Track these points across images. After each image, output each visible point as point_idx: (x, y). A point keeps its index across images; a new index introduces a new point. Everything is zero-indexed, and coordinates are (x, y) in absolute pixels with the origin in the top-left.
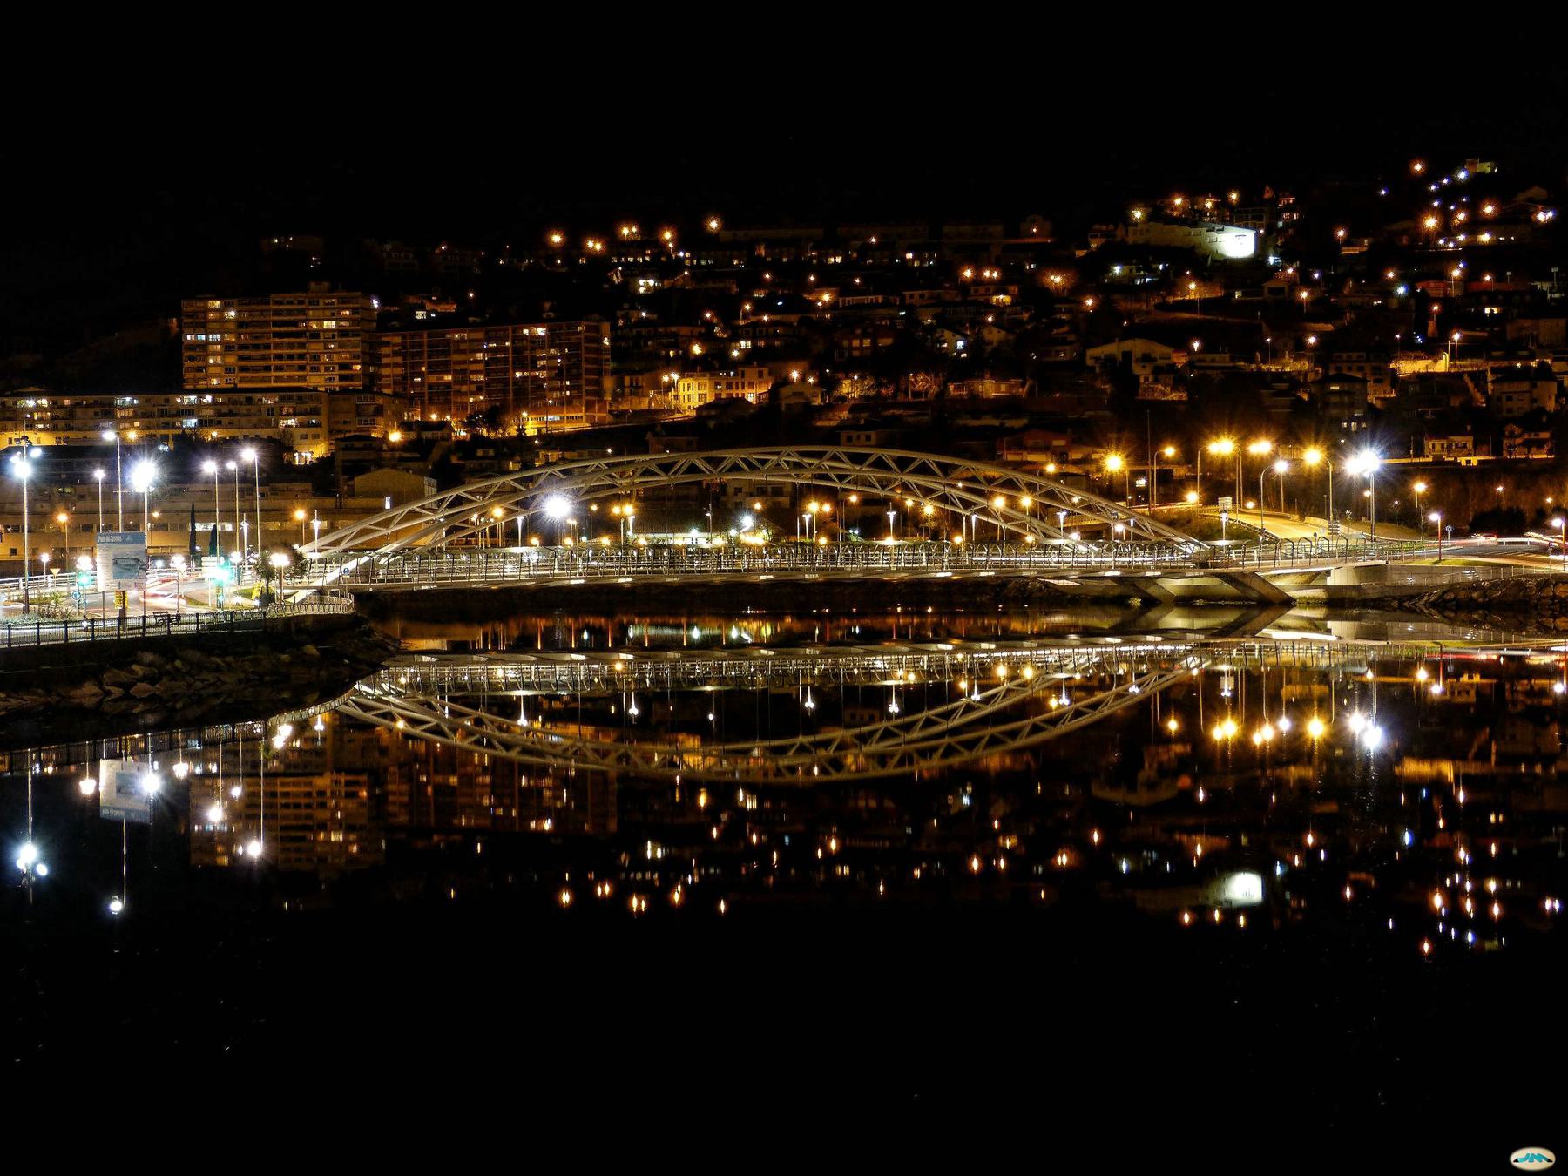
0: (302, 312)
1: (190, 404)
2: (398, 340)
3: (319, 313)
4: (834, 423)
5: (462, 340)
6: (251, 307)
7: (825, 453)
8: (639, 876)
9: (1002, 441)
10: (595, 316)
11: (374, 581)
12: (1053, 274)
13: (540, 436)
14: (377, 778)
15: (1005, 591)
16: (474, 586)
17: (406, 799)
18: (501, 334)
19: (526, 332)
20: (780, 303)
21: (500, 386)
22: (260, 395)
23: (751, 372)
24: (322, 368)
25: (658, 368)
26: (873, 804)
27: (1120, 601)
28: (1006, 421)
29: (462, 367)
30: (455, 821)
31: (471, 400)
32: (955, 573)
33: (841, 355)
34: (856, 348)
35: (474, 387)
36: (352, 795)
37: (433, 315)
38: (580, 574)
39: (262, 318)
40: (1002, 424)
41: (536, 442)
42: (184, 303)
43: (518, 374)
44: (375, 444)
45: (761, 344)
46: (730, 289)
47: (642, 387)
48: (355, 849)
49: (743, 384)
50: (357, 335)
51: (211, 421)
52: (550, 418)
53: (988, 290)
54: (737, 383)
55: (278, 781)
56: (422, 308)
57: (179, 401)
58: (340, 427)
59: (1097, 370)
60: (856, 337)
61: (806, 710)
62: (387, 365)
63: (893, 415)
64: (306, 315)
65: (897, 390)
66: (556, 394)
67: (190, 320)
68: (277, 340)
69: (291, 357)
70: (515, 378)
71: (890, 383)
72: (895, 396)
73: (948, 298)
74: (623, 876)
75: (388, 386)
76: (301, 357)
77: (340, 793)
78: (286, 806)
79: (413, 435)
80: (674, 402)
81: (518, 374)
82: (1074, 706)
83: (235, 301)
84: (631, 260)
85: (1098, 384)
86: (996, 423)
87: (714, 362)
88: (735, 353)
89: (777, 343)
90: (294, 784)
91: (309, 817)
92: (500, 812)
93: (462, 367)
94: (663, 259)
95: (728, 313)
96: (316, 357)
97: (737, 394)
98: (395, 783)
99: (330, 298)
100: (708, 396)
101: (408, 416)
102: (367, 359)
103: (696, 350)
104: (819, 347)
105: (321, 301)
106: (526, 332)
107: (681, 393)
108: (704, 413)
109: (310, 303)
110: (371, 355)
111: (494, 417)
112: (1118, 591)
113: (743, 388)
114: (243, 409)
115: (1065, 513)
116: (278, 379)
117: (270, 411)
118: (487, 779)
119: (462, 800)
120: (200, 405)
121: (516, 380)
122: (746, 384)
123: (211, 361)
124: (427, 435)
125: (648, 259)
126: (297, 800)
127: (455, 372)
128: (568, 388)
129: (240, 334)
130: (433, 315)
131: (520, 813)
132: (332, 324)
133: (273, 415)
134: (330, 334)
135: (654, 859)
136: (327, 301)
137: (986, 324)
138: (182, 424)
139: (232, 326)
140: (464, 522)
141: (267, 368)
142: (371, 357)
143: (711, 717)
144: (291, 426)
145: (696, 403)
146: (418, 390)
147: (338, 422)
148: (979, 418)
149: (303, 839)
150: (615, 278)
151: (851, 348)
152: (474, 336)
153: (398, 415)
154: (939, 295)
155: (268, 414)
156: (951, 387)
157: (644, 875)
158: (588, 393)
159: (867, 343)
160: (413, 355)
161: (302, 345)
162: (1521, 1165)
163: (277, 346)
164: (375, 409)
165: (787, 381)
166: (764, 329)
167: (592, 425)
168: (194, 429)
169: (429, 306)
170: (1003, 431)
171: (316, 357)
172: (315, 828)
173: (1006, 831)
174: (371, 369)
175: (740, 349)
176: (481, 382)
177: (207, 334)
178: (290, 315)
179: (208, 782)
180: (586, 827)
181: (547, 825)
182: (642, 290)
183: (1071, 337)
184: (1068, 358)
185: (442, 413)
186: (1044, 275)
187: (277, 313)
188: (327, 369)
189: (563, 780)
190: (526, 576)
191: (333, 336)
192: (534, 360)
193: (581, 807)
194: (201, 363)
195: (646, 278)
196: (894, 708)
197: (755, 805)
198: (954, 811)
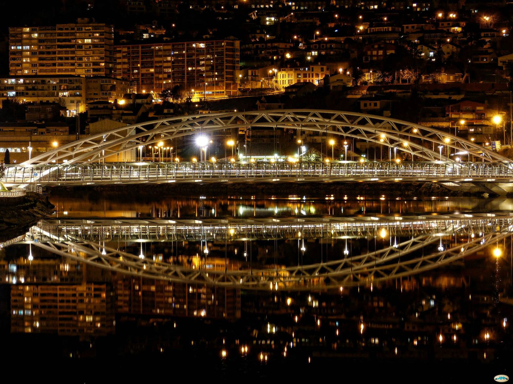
0: (73, 34)
1: (12, 84)
2: (125, 49)
3: (83, 35)
4: (359, 96)
5: (160, 50)
6: (45, 32)
7: (309, 113)
8: (263, 342)
9: (449, 107)
10: (232, 37)
11: (61, 180)
12: (485, 16)
13: (201, 103)
14: (111, 286)
15: (421, 189)
16: (115, 183)
17: (127, 298)
18: (181, 47)
19: (194, 45)
20: (336, 31)
21: (180, 75)
22: (49, 79)
23: (317, 69)
24: (84, 65)
25: (266, 66)
26: (381, 304)
27: (479, 195)
28: (452, 96)
29: (161, 64)
30: (154, 311)
31: (164, 82)
32: (381, 179)
33: (367, 59)
34: (375, 56)
35: (166, 76)
36: (97, 296)
37: (152, 36)
38: (174, 177)
39: (52, 38)
40: (450, 98)
41: (197, 106)
42: (10, 29)
43: (190, 69)
44: (109, 106)
45: (323, 53)
46: (316, 23)
47: (258, 76)
48: (99, 325)
49: (313, 74)
50: (103, 47)
51: (23, 93)
52: (207, 92)
53: (449, 24)
54: (309, 74)
55: (58, 287)
56: (146, 32)
57: (6, 82)
58: (93, 96)
59: (504, 69)
60: (375, 49)
61: (301, 252)
62: (120, 63)
63: (391, 92)
64: (75, 36)
65: (394, 78)
66: (210, 80)
67: (14, 38)
68: (59, 49)
69: (67, 58)
70: (188, 70)
71: (390, 75)
72: (392, 81)
73: (427, 28)
74: (255, 342)
75: (120, 75)
76: (72, 58)
77: (91, 295)
78: (62, 301)
79: (131, 101)
80: (275, 84)
81: (190, 69)
82: (446, 251)
83: (38, 28)
84: (262, 6)
85: (504, 76)
86: (447, 97)
87: (297, 63)
88: (309, 58)
89: (332, 53)
90: (67, 289)
91: (75, 307)
92: (178, 306)
93: (161, 64)
94: (280, 6)
95: (307, 35)
96: (80, 59)
97: (309, 80)
98: (121, 289)
99: (89, 26)
100: (293, 81)
101: (130, 91)
102: (108, 60)
103: (288, 56)
104: (355, 55)
105: (83, 28)
106: (194, 45)
107: (279, 79)
108: (290, 90)
109: (78, 29)
110: (110, 58)
111: (176, 92)
112: (477, 189)
113: (313, 77)
114: (40, 87)
115: (442, 147)
116: (59, 70)
117: (55, 88)
118: (171, 288)
119: (157, 300)
120: (17, 84)
121: (188, 72)
122: (314, 75)
123: (24, 61)
124: (139, 101)
125: (271, 6)
126: (68, 298)
127: (156, 67)
128: (217, 76)
129: (40, 46)
130: (152, 36)
131: (188, 307)
132: (89, 41)
133: (56, 90)
134: (88, 47)
135: (271, 333)
136: (87, 28)
137: (445, 43)
138: (7, 94)
139: (36, 41)
140: (432, 239)
141: (54, 65)
142: (110, 59)
143: (245, 254)
144: (65, 96)
145: (287, 85)
146: (136, 77)
147: (91, 94)
148: (437, 94)
149: (71, 319)
150: (253, 16)
151: (372, 56)
152: (166, 47)
153: (125, 90)
154: (422, 26)
155: (53, 90)
156: (423, 77)
157: (266, 342)
158: (227, 79)
159: (381, 53)
160: (133, 58)
161: (73, 52)
162: (498, 381)
163: (60, 52)
164: (111, 87)
165: (337, 73)
166: (325, 45)
167: (229, 96)
168: (13, 97)
169: (150, 31)
170: (451, 101)
171: (80, 59)
172: (78, 313)
173: (455, 320)
174: (110, 65)
175: (311, 56)
176: (170, 72)
177: (22, 46)
178: (67, 36)
179: (21, 288)
180: (224, 315)
181: (203, 313)
182: (268, 23)
183: (490, 51)
184: (488, 62)
185: (148, 90)
186: (480, 16)
187: (60, 34)
188: (86, 65)
189: (212, 289)
190: (144, 178)
191: (90, 47)
192: (198, 61)
193: (221, 304)
194: (19, 62)
195: (270, 16)
196: (346, 252)
197: (317, 304)
198: (426, 309)
